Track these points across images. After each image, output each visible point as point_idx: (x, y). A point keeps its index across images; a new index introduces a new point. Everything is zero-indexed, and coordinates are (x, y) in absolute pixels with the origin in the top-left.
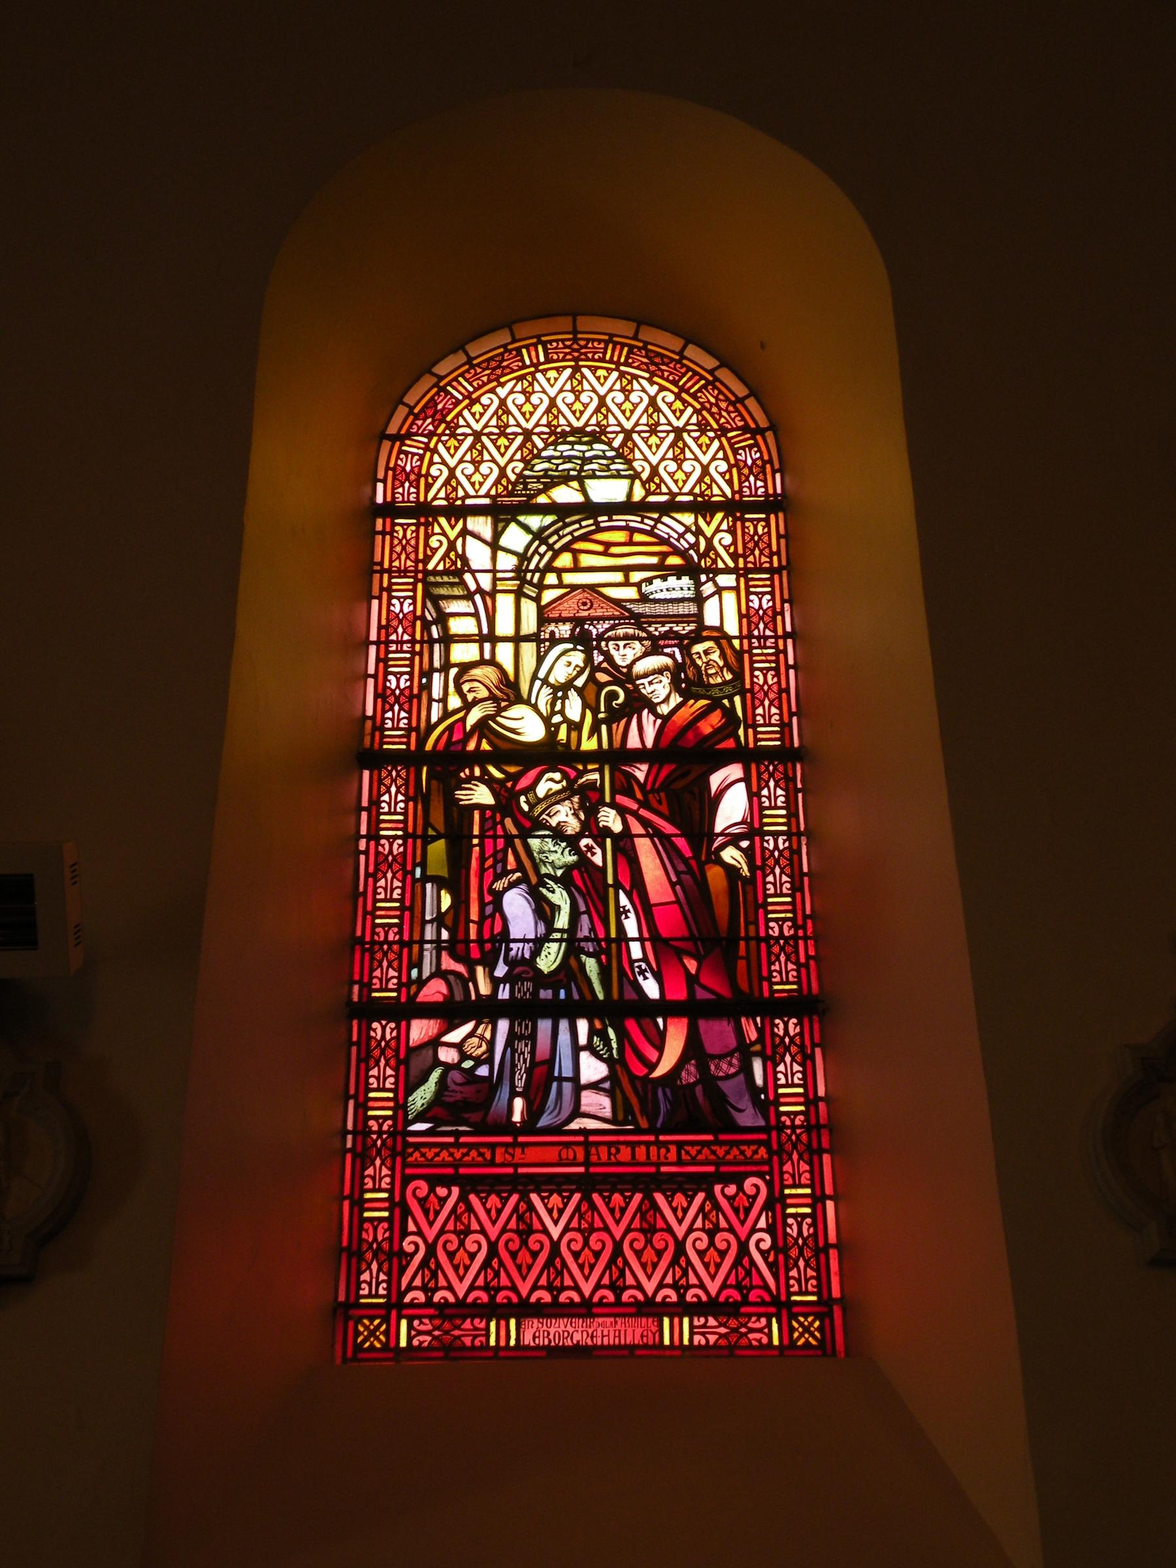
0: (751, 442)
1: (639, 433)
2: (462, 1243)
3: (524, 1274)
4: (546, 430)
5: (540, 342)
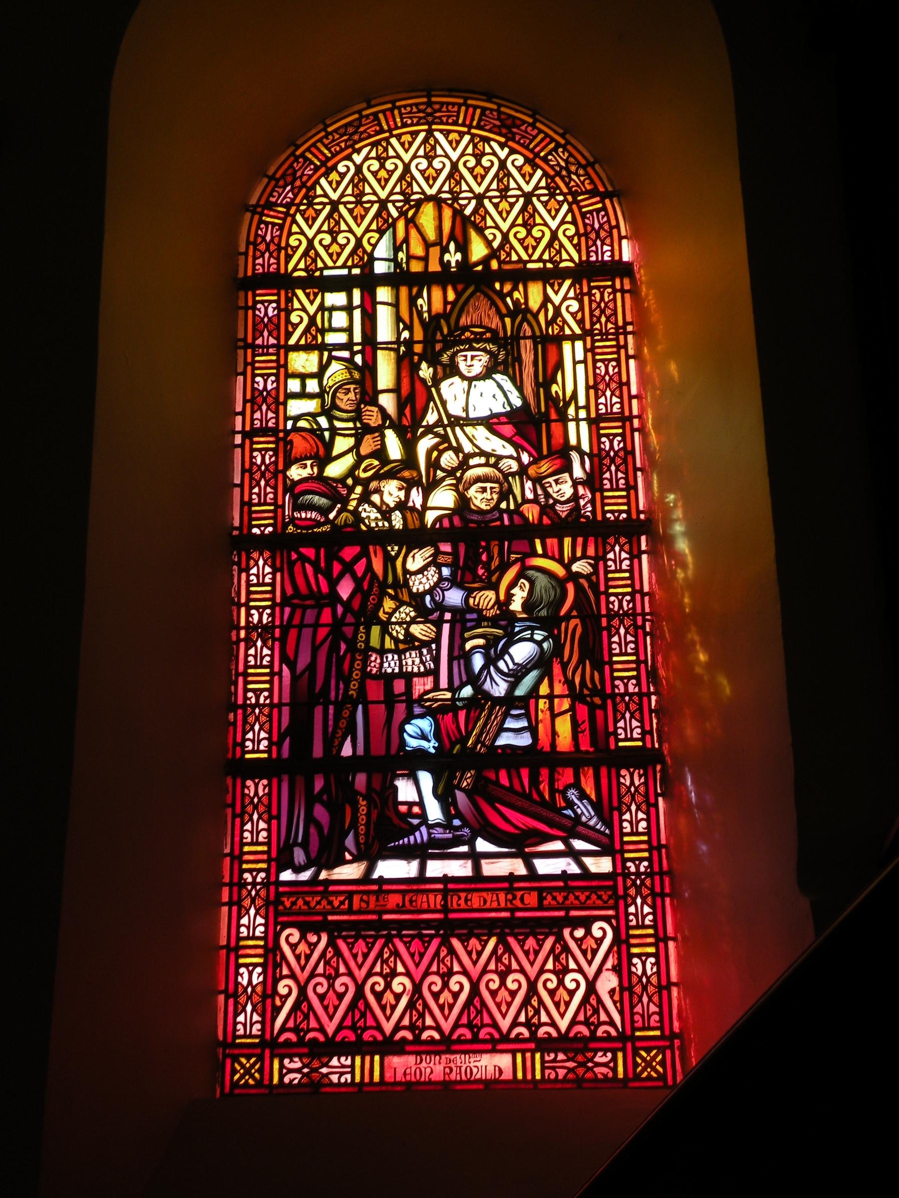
1: (345, 204)
2: (503, 983)
3: (504, 1011)
4: (401, 197)
5: (465, 104)
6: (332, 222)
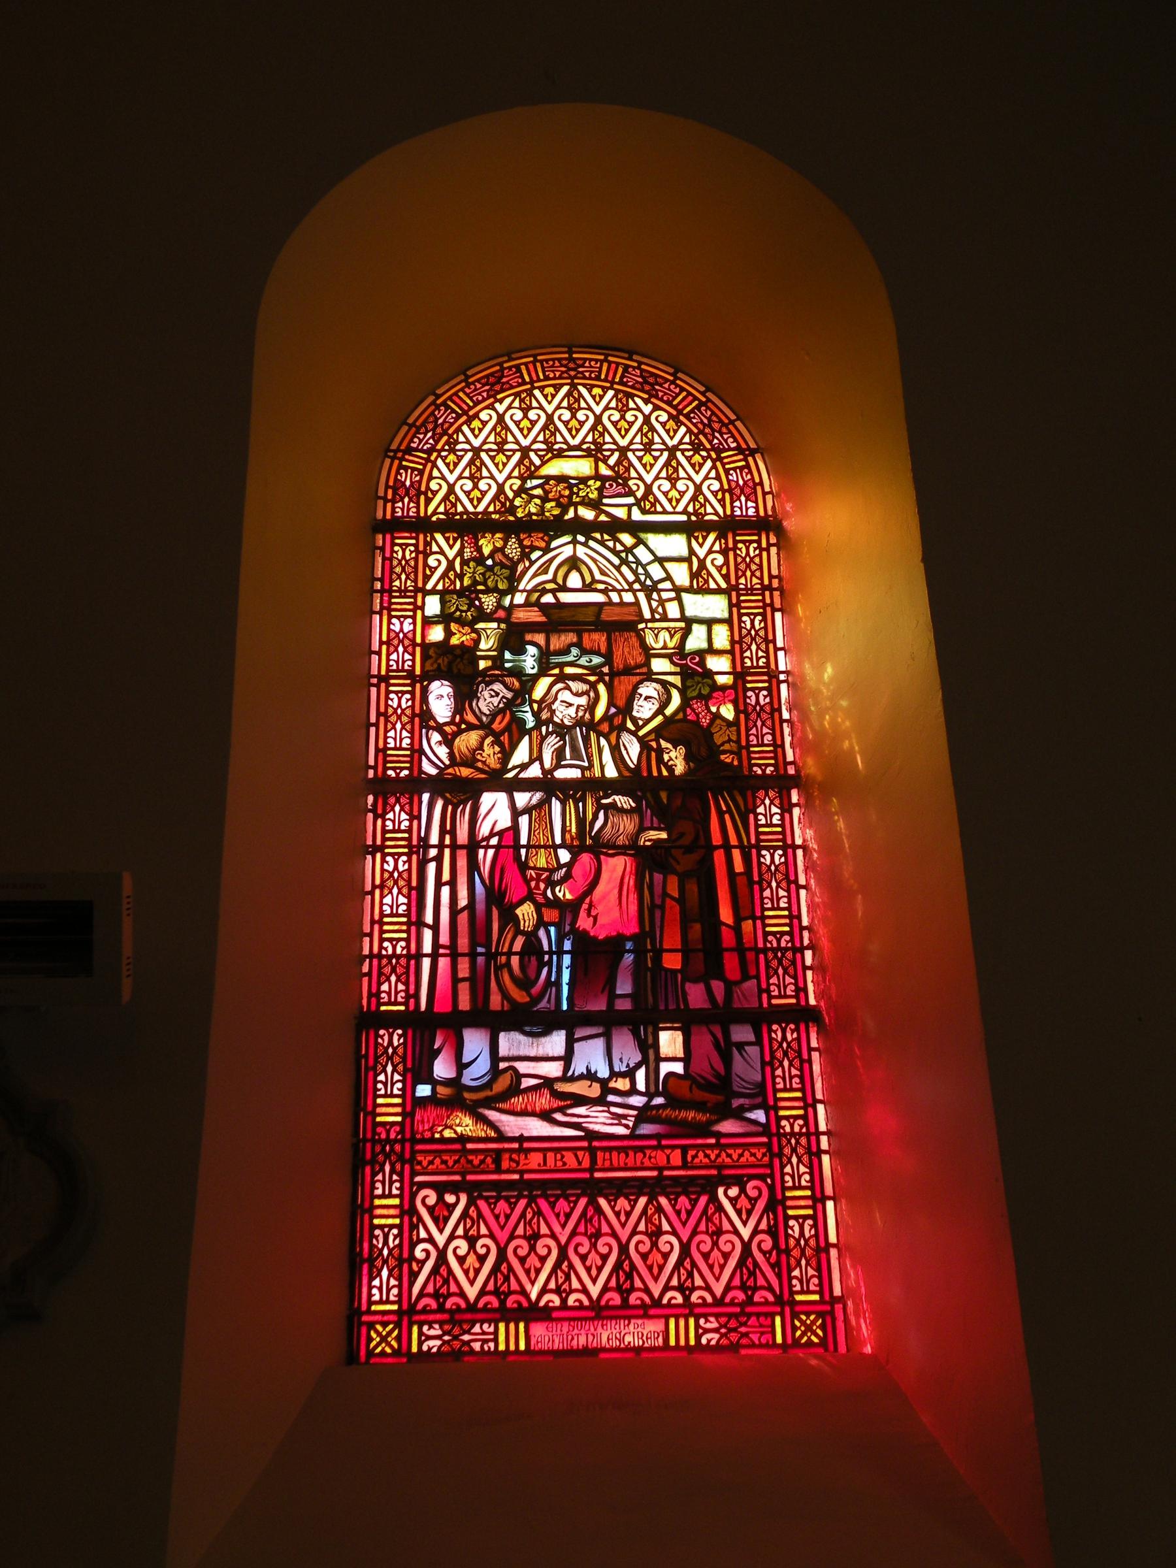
0: (743, 463)
2: (715, 1244)
4: (543, 446)
6: (474, 469)
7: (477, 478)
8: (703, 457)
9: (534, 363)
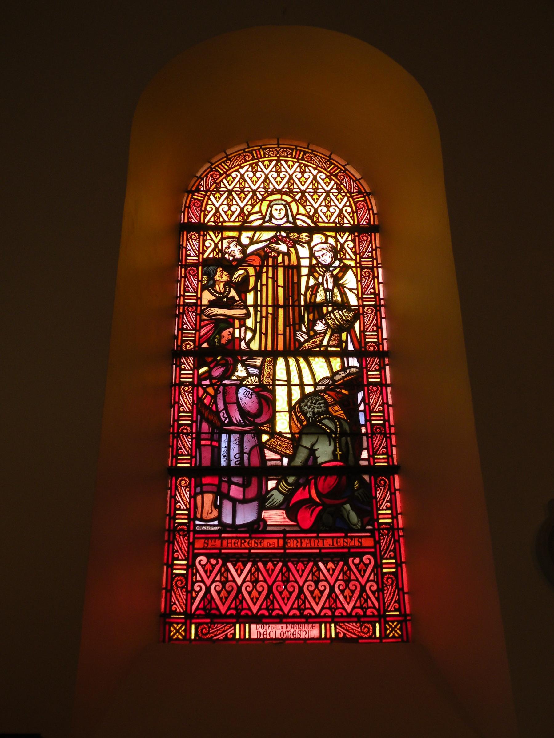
3: (224, 602)
4: (263, 190)
5: (261, 148)
7: (328, 206)
8: (342, 196)
9: (259, 150)
